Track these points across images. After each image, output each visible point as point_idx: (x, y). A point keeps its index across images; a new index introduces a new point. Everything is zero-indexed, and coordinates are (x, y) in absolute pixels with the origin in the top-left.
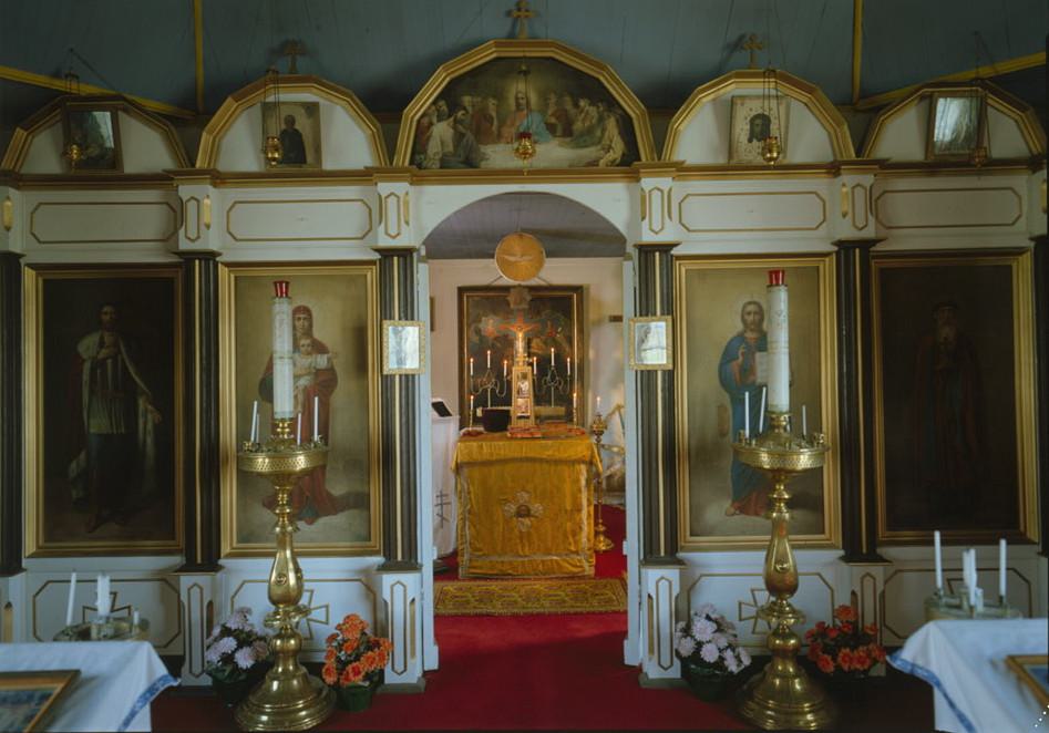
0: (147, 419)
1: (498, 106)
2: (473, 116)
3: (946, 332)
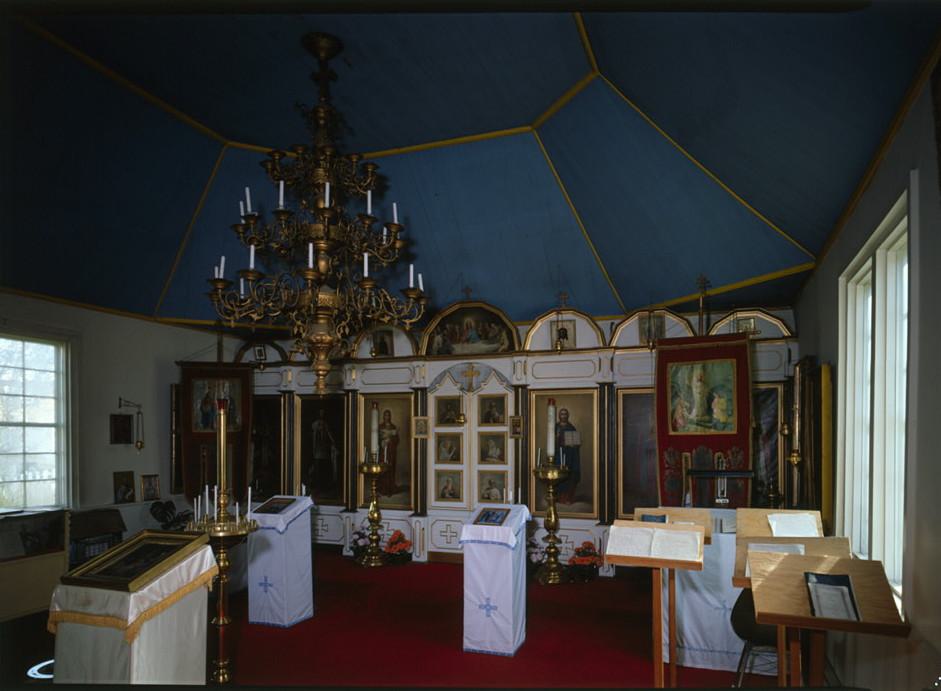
0: (334, 455)
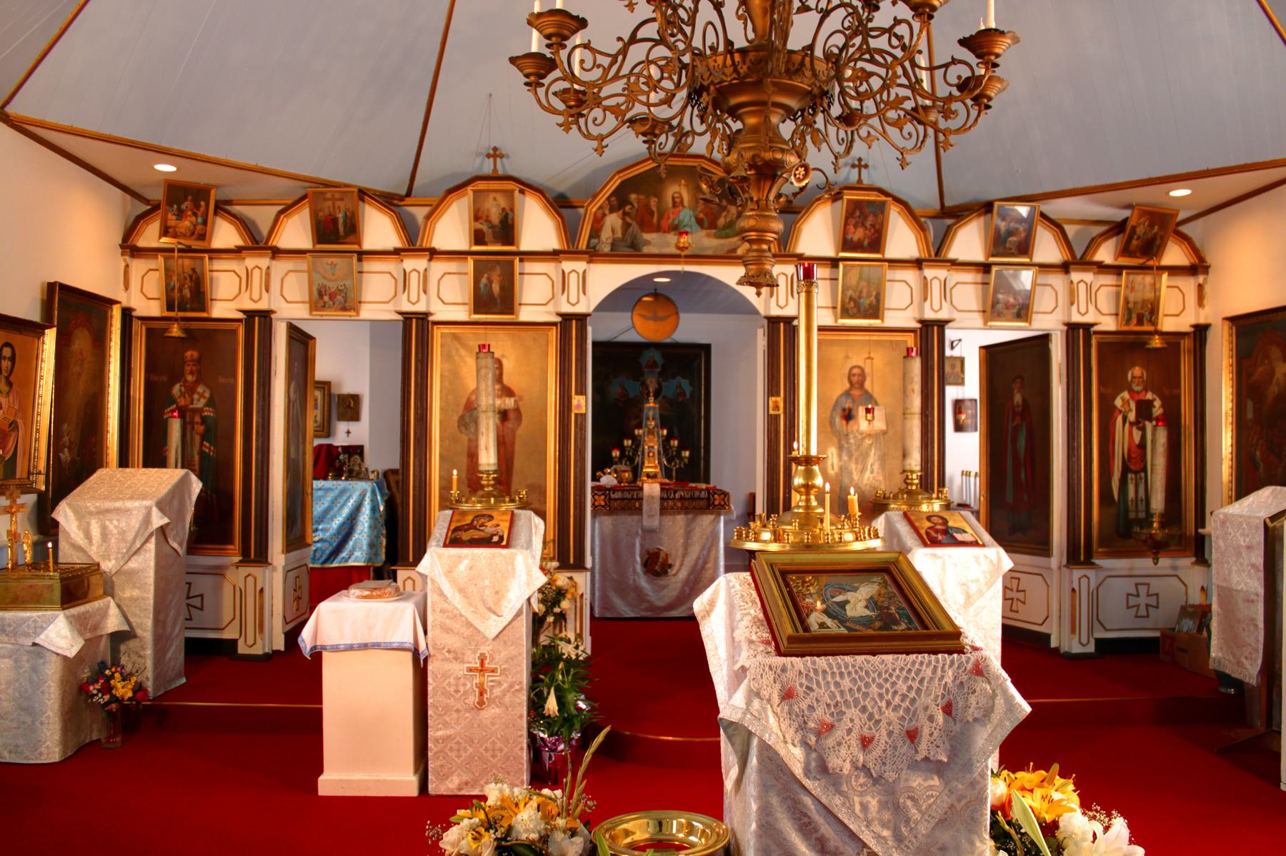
1: (658, 203)
2: (637, 210)
3: (1018, 398)
